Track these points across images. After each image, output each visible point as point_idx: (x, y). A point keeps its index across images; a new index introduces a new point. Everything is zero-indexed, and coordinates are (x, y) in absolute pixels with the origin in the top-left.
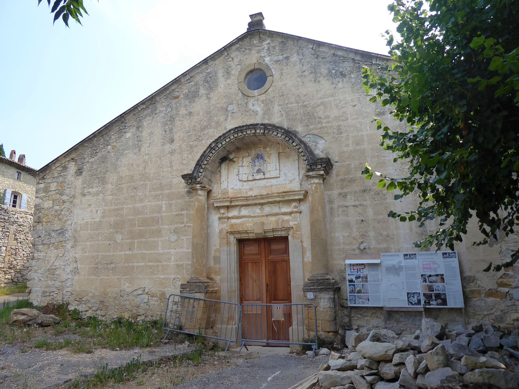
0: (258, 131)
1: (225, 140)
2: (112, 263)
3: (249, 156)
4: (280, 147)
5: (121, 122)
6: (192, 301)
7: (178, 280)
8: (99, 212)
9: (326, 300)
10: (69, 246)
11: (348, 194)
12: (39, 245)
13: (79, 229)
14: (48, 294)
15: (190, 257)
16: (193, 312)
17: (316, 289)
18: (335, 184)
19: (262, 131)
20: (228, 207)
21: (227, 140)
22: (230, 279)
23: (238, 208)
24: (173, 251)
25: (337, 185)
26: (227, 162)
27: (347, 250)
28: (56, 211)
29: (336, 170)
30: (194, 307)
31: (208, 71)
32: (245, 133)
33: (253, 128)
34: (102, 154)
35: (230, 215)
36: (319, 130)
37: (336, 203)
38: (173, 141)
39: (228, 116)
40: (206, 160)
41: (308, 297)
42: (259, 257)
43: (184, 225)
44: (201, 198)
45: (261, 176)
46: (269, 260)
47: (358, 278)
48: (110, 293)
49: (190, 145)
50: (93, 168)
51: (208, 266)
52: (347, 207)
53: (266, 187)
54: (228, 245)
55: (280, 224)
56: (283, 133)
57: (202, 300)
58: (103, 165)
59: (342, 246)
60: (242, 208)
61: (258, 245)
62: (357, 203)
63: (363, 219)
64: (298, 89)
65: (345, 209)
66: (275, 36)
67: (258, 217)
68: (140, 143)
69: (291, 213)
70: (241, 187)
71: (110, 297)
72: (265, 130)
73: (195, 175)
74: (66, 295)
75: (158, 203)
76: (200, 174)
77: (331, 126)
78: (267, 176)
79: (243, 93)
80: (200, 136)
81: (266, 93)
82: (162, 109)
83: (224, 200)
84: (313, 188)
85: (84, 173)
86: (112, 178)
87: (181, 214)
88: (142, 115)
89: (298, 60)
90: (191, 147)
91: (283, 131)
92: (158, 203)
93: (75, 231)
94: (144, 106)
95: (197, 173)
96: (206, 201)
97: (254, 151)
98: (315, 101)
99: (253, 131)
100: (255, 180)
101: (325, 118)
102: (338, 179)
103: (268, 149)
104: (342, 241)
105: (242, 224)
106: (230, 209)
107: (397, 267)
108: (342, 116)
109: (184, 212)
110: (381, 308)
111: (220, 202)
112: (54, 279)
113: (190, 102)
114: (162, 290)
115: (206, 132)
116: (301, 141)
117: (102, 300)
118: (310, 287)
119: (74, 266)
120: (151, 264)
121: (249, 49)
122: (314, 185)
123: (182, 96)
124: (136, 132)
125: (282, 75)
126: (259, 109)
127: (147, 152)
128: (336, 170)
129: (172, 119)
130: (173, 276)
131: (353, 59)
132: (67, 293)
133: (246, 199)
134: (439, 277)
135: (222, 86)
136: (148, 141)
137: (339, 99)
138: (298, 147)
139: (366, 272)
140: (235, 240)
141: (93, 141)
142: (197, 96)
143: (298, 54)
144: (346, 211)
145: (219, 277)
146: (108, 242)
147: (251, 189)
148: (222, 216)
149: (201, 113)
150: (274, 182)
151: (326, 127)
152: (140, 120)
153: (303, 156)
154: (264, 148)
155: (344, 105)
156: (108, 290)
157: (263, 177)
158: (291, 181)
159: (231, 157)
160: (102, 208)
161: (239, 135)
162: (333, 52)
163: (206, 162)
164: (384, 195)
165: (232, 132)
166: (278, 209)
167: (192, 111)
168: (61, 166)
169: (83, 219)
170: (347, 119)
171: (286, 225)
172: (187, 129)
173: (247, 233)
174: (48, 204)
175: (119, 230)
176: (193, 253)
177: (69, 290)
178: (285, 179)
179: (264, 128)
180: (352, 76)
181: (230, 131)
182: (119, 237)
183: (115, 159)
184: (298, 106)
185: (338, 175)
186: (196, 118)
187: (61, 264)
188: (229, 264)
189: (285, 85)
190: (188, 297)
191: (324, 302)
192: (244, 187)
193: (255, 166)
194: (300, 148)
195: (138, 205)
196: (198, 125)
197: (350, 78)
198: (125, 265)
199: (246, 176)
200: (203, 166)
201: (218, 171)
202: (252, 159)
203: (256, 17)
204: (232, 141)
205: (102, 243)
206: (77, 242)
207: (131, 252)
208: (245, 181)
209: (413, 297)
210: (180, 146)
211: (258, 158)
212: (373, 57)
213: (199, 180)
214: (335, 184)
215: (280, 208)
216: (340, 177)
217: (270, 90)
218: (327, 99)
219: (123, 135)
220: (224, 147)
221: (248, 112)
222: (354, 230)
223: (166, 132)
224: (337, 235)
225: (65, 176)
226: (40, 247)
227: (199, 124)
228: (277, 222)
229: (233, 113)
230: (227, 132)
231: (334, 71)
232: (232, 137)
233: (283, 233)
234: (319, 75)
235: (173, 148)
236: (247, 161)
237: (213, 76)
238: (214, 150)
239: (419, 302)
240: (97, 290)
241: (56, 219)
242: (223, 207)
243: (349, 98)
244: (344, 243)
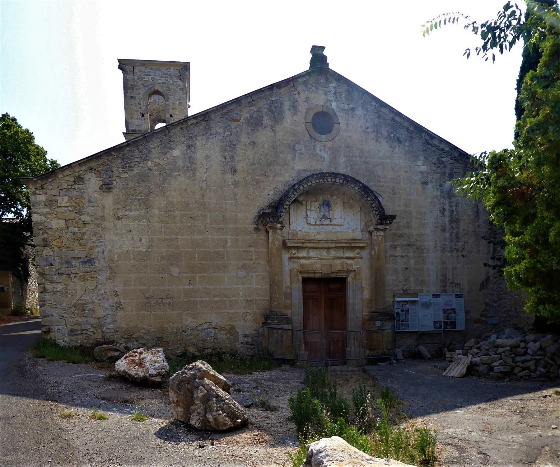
0: (338, 181)
1: (307, 184)
2: (167, 298)
3: (317, 201)
5: (164, 134)
7: (248, 314)
8: (143, 240)
10: (103, 277)
12: (52, 275)
13: (116, 259)
14: (79, 332)
19: (341, 181)
20: (298, 248)
21: (309, 184)
24: (241, 287)
26: (296, 203)
28: (74, 234)
31: (273, 99)
32: (326, 180)
33: (333, 177)
34: (140, 170)
36: (378, 188)
37: (388, 253)
38: (235, 171)
39: (295, 156)
45: (328, 222)
47: (402, 311)
48: (169, 328)
49: (255, 179)
50: (129, 186)
52: (396, 256)
55: (345, 267)
58: (144, 185)
59: (391, 288)
62: (403, 254)
63: (406, 267)
64: (362, 145)
65: (395, 258)
66: (342, 81)
67: (326, 259)
68: (194, 166)
69: (353, 258)
71: (169, 332)
74: (108, 333)
75: (221, 237)
78: (334, 222)
79: (310, 135)
80: (266, 172)
81: (333, 141)
82: (219, 131)
83: (299, 241)
84: (380, 239)
85: (115, 190)
86: (158, 202)
87: (250, 251)
88: (192, 132)
89: (363, 115)
92: (221, 237)
93: (112, 260)
94: (195, 121)
99: (333, 180)
100: (323, 225)
103: (334, 197)
104: (391, 283)
107: (428, 303)
110: (417, 332)
111: (294, 242)
112: (85, 315)
113: (252, 130)
114: (232, 324)
115: (272, 168)
117: (160, 336)
119: (115, 301)
120: (217, 299)
121: (315, 87)
122: (381, 237)
123: (242, 121)
124: (187, 151)
125: (347, 126)
126: (326, 156)
127: (204, 179)
129: (232, 146)
130: (243, 311)
131: (407, 128)
132: (108, 330)
134: (453, 310)
135: (289, 121)
136: (205, 165)
138: (371, 202)
139: (408, 307)
141: (123, 151)
142: (261, 124)
143: (363, 109)
146: (161, 275)
147: (318, 233)
148: (292, 255)
149: (266, 146)
150: (338, 229)
151: (383, 186)
152: (190, 137)
153: (376, 211)
156: (166, 326)
157: (330, 223)
158: (354, 231)
160: (147, 236)
161: (320, 181)
162: (392, 115)
164: (423, 250)
167: (256, 141)
168: (72, 176)
169: (121, 247)
171: (350, 268)
172: (251, 161)
174: (58, 223)
175: (174, 262)
177: (111, 326)
180: (406, 144)
182: (175, 271)
183: (161, 179)
187: (94, 298)
189: (350, 137)
195: (196, 237)
197: (405, 145)
198: (185, 300)
203: (318, 50)
205: (152, 275)
206: (115, 273)
207: (191, 287)
209: (437, 324)
212: (424, 131)
215: (343, 253)
217: (336, 138)
219: (168, 152)
221: (315, 156)
222: (400, 275)
223: (226, 159)
225: (82, 191)
226: (55, 277)
228: (342, 264)
231: (392, 135)
233: (344, 274)
234: (380, 135)
235: (237, 179)
236: (315, 206)
237: (278, 106)
239: (440, 327)
240: (151, 326)
241: (76, 244)
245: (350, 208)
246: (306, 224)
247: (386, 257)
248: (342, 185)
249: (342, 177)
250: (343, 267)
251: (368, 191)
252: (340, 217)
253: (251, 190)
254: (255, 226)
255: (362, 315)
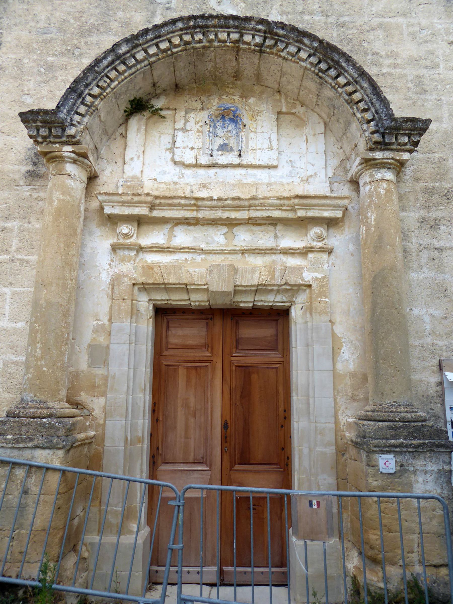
0: (247, 38)
1: (157, 45)
3: (203, 109)
4: (283, 101)
6: (20, 473)
9: (429, 478)
11: (443, 221)
15: (23, 342)
16: (22, 507)
17: (406, 447)
18: (412, 198)
19: (258, 40)
21: (164, 45)
22: (133, 406)
23: (166, 228)
25: (416, 199)
26: (147, 114)
27: (441, 350)
29: (412, 167)
30: (25, 492)
32: (212, 37)
33: (236, 27)
35: (145, 241)
37: (414, 240)
40: (98, 86)
41: (382, 467)
42: (208, 354)
43: (8, 257)
44: (70, 182)
45: (232, 158)
46: (231, 363)
49: (47, 62)
51: (71, 369)
52: (439, 250)
53: (240, 184)
54: (134, 317)
56: (316, 49)
57: (55, 470)
59: (429, 340)
60: (176, 228)
61: (207, 324)
65: (436, 254)
67: (220, 252)
70: (176, 180)
72: (265, 38)
73: (62, 115)
76: (77, 118)
77: (401, 76)
78: (247, 159)
80: (76, 47)
83: (136, 199)
84: (382, 192)
90: (50, 68)
91: (316, 44)
95: (69, 112)
96: (83, 197)
97: (216, 100)
98: (366, 19)
99: (235, 36)
100: (215, 165)
101: (388, 57)
102: (418, 188)
103: (252, 100)
104: (428, 327)
105: (177, 266)
106: (144, 228)
108: (425, 59)
109: (14, 224)
111: (123, 203)
116: (363, 74)
118: (387, 439)
122: (385, 185)
128: (412, 167)
133: (195, 205)
137: (419, 24)
138: (350, 89)
140: (151, 307)
144: (437, 260)
145: (102, 401)
148: (122, 241)
151: (389, 74)
153: (365, 110)
154: (242, 97)
155: (429, 38)
157: (236, 161)
159: (158, 103)
163: (96, 91)
165: (180, 25)
166: (272, 239)
170: (437, 66)
171: (293, 280)
172: (42, 24)
173: (188, 290)
176: (33, 332)
178: (291, 172)
179: (265, 32)
181: (174, 21)
184: (326, 23)
185: (417, 180)
186: (68, 3)
188: (132, 366)
190: (8, 463)
191: (426, 482)
192: (187, 180)
193: (215, 135)
194: (355, 92)
196: (72, 21)
199: (193, 154)
200: (89, 99)
201: (118, 134)
202: (210, 117)
204: (175, 50)
208: (189, 166)
210: (18, 61)
211: (223, 117)
213: (72, 131)
214: (412, 198)
215: (276, 237)
216: (423, 184)
218: (392, 20)
220: (150, 64)
224: (416, 311)
227: (76, 19)
228: (271, 270)
229: (168, 9)
230: (165, 24)
232: (176, 41)
233: (279, 298)
238: (125, 64)
242: (128, 219)
243: (440, 26)
244: (433, 333)
245: (297, 126)
246: (171, 164)
247: (405, 251)
248: (261, 52)
249: (260, 27)
250: (273, 275)
251: (336, 57)
252: (266, 146)
253: (31, 85)
254: (30, 168)
255: (336, 423)
